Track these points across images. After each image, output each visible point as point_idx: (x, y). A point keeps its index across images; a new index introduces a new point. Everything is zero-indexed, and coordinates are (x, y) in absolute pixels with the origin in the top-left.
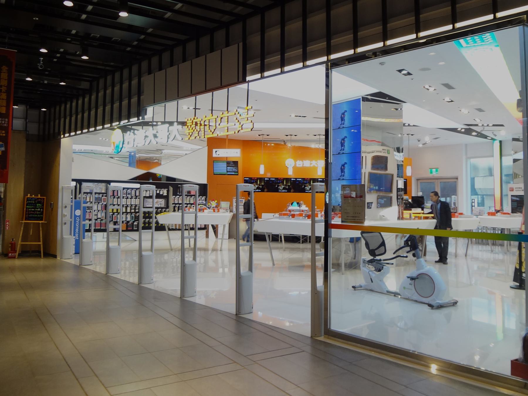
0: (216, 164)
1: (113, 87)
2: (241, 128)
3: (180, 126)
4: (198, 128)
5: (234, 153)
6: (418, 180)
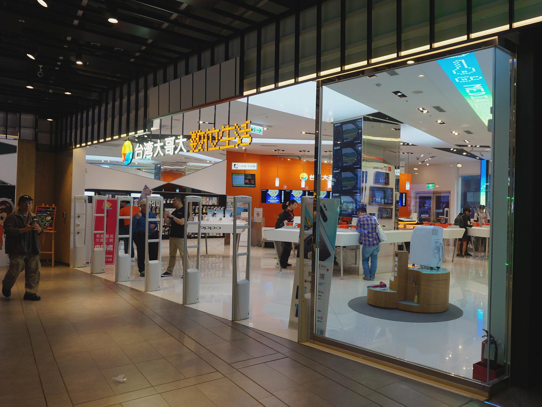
0: (234, 176)
1: (114, 96)
3: (185, 140)
4: (202, 142)
5: (251, 167)
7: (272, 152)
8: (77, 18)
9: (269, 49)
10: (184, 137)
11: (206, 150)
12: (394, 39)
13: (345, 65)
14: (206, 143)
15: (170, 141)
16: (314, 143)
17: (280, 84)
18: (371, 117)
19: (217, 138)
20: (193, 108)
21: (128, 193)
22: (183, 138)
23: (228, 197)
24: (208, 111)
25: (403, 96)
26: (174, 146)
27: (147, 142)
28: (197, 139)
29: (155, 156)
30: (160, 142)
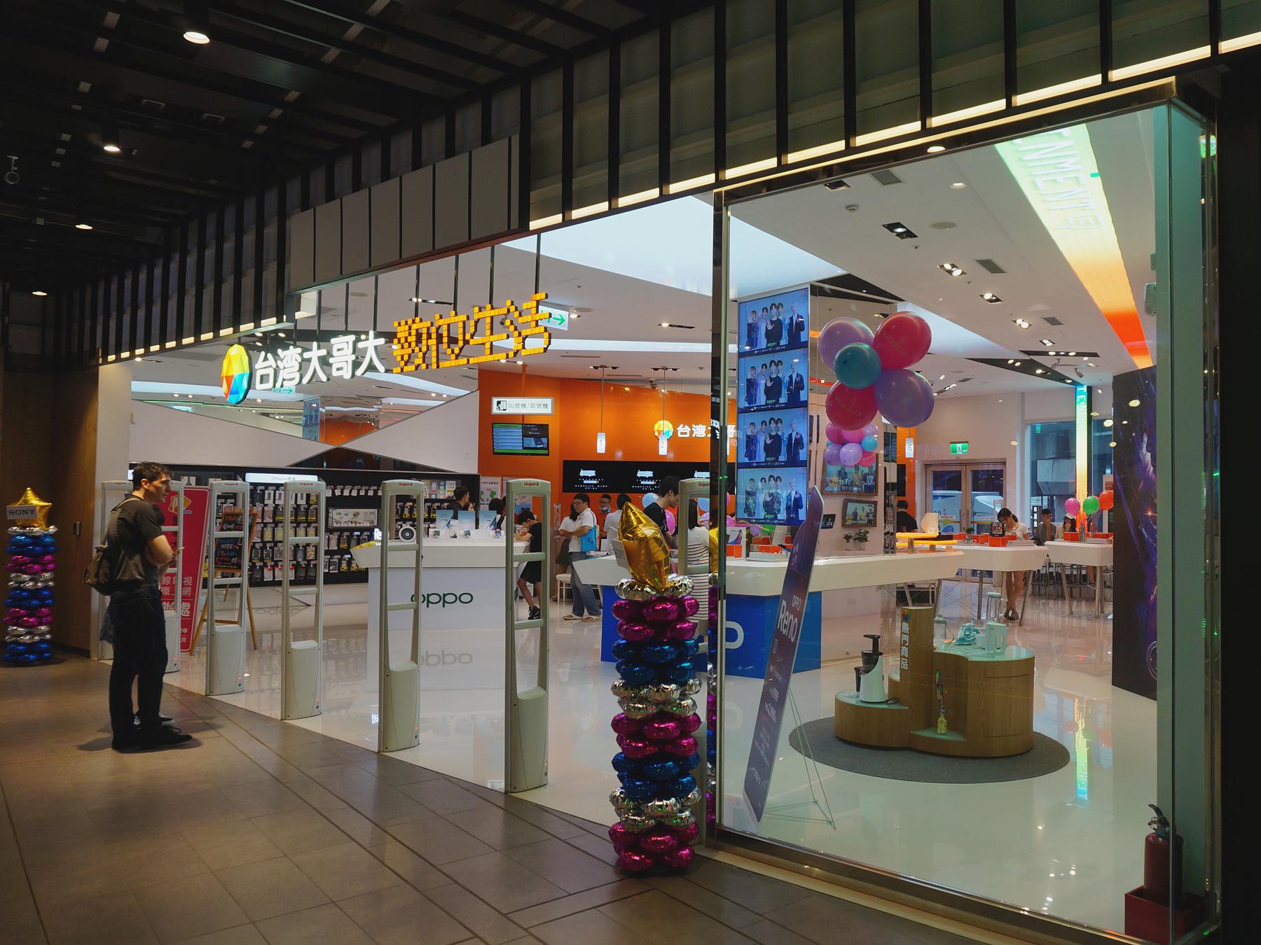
2: (520, 347)
3: (382, 341)
5: (537, 406)
6: (927, 466)
7: (588, 371)
8: (106, 33)
9: (593, 117)
10: (378, 335)
11: (434, 366)
12: (838, 108)
13: (787, 152)
14: (434, 348)
15: (342, 346)
16: (710, 350)
17: (623, 201)
18: (826, 286)
19: (460, 337)
20: (402, 262)
21: (237, 472)
22: (378, 335)
23: (483, 479)
24: (438, 270)
25: (909, 234)
26: (353, 357)
27: (286, 348)
28: (412, 339)
29: (305, 381)
30: (319, 348)
